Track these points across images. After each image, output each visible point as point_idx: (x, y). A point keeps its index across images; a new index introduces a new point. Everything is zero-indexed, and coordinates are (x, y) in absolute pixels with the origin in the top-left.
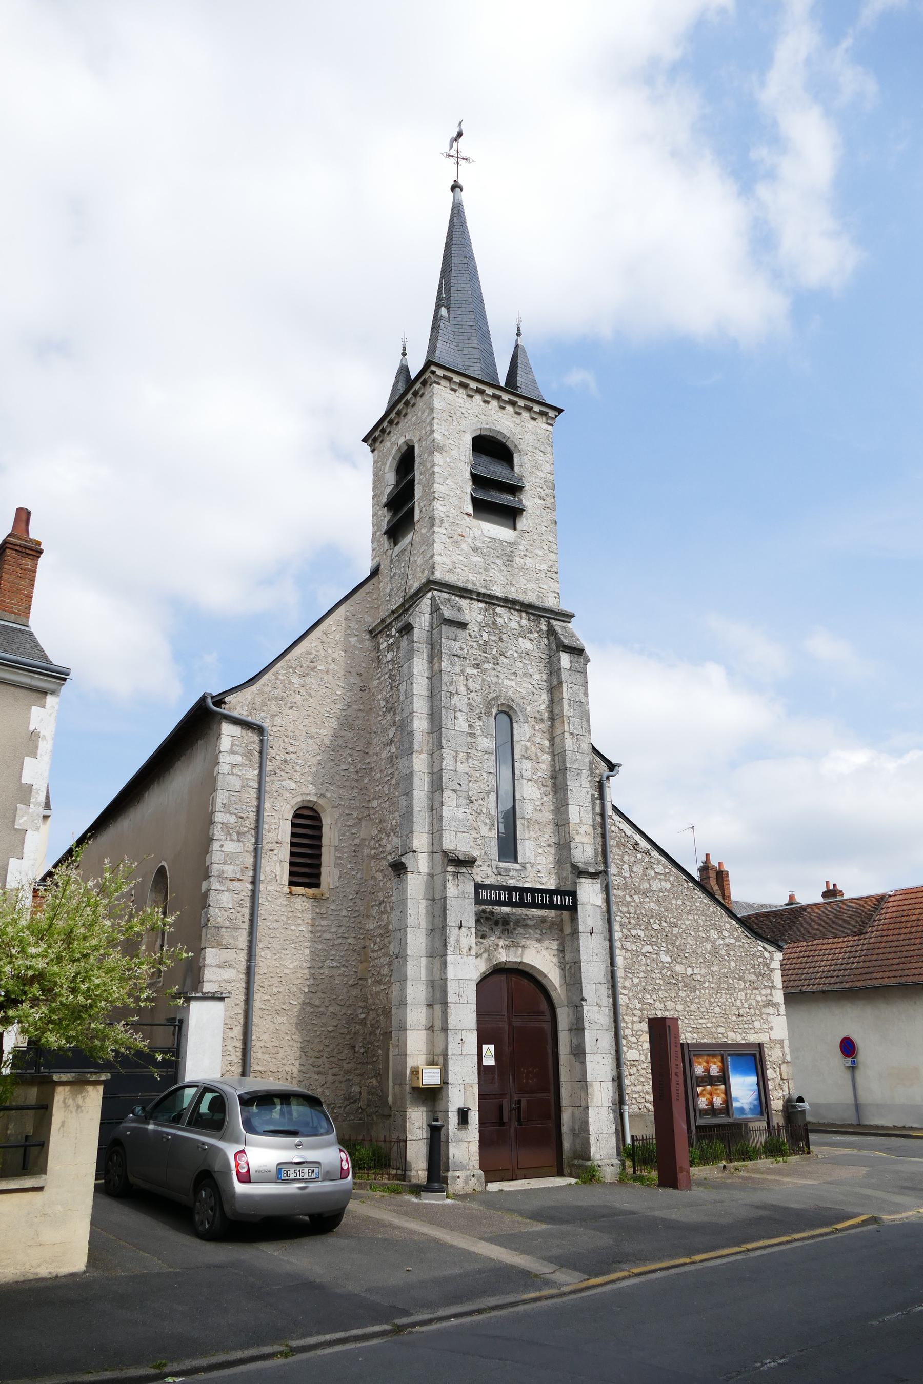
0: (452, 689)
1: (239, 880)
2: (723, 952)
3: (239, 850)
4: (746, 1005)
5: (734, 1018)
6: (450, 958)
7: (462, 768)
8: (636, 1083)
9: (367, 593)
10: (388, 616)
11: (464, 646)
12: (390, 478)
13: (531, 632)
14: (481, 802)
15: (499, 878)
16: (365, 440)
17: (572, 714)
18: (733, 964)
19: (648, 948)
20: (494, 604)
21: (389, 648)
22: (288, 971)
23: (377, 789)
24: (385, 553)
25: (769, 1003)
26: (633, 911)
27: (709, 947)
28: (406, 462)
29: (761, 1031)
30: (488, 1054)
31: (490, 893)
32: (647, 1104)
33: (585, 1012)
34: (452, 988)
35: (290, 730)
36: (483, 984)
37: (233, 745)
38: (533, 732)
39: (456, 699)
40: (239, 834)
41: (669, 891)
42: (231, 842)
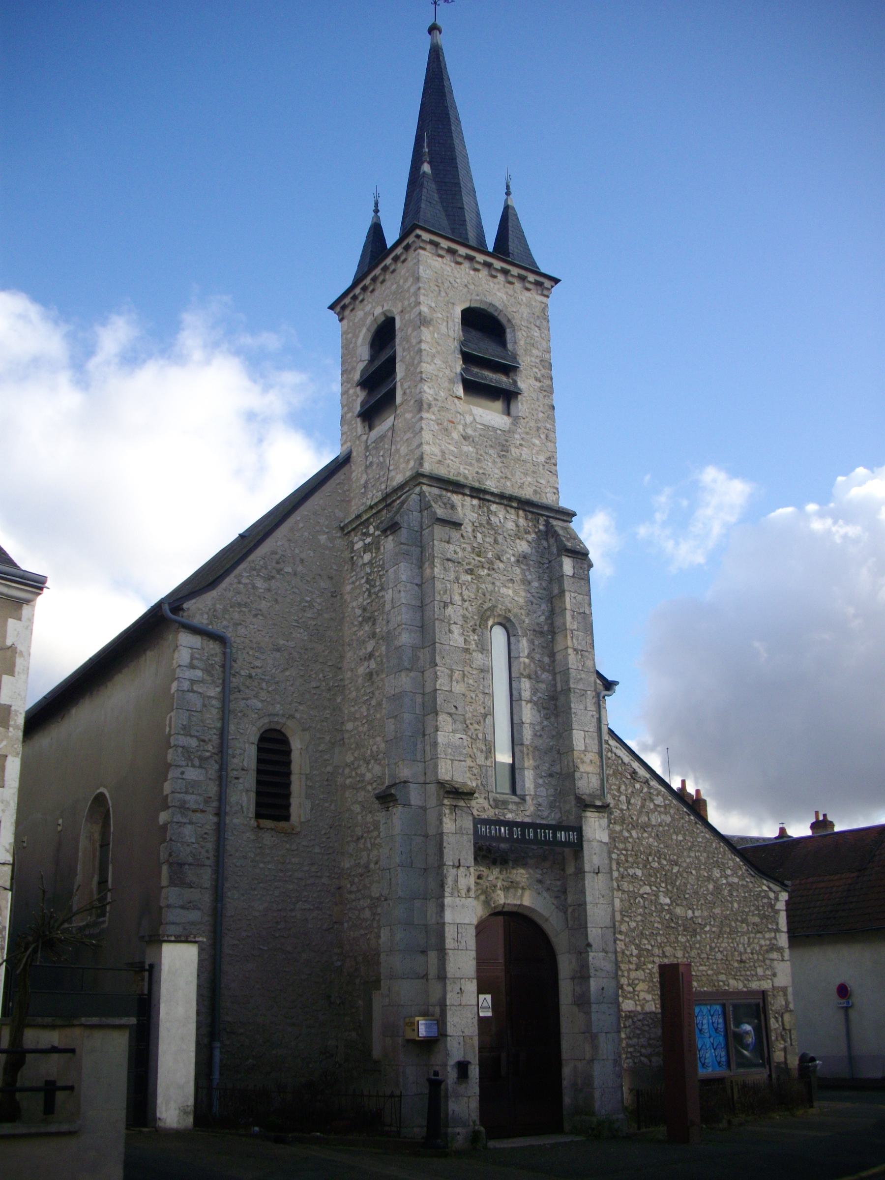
0: (446, 598)
1: (203, 811)
2: (726, 892)
3: (202, 778)
4: (749, 950)
5: (736, 965)
6: (448, 900)
7: (458, 688)
8: (631, 1035)
9: (339, 484)
10: (366, 511)
11: (458, 550)
12: (363, 352)
13: (528, 533)
14: (477, 727)
15: (497, 811)
16: (332, 307)
17: (575, 627)
18: (736, 905)
19: (647, 889)
20: (489, 501)
21: (367, 548)
22: (257, 914)
23: (353, 709)
24: (359, 437)
25: (773, 948)
26: (630, 848)
27: (711, 887)
28: (384, 334)
29: (764, 978)
30: (485, 1004)
31: (490, 828)
32: (642, 1058)
33: (590, 958)
34: (450, 933)
35: (254, 641)
36: (481, 928)
37: (192, 658)
38: (532, 647)
39: (450, 610)
40: (201, 759)
41: (668, 825)
42: (192, 769)
